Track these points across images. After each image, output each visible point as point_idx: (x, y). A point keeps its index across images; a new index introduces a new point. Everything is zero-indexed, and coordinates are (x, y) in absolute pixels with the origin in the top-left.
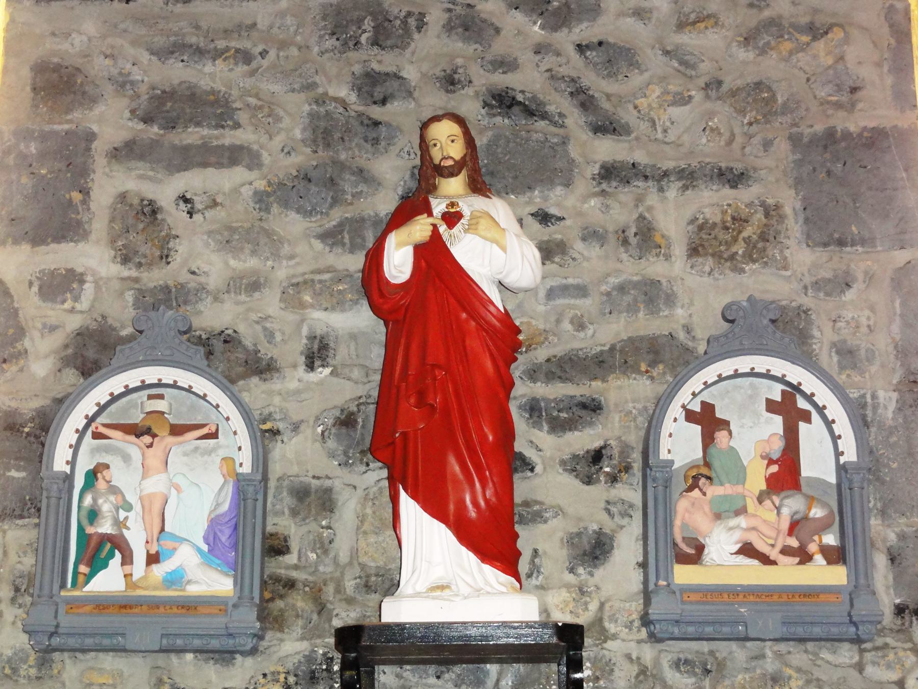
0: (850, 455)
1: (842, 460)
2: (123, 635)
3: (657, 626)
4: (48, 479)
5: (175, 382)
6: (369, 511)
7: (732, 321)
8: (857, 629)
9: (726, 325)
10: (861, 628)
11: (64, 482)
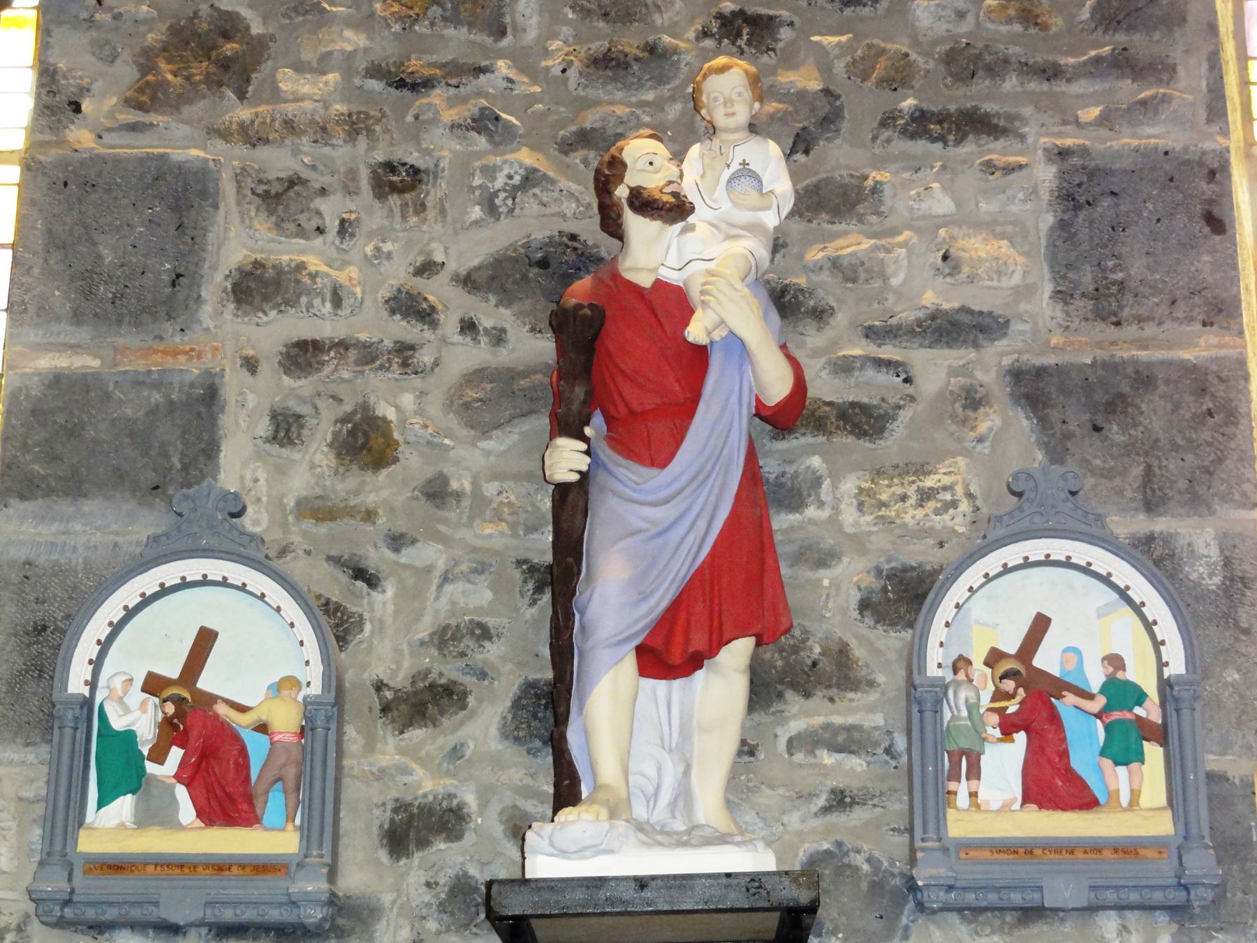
0: (1177, 666)
1: (1167, 672)
2: (156, 904)
3: (925, 894)
4: (61, 703)
5: (225, 578)
6: (871, 802)
7: (1019, 495)
8: (1189, 893)
9: (1015, 499)
10: (1193, 893)
11: (82, 708)
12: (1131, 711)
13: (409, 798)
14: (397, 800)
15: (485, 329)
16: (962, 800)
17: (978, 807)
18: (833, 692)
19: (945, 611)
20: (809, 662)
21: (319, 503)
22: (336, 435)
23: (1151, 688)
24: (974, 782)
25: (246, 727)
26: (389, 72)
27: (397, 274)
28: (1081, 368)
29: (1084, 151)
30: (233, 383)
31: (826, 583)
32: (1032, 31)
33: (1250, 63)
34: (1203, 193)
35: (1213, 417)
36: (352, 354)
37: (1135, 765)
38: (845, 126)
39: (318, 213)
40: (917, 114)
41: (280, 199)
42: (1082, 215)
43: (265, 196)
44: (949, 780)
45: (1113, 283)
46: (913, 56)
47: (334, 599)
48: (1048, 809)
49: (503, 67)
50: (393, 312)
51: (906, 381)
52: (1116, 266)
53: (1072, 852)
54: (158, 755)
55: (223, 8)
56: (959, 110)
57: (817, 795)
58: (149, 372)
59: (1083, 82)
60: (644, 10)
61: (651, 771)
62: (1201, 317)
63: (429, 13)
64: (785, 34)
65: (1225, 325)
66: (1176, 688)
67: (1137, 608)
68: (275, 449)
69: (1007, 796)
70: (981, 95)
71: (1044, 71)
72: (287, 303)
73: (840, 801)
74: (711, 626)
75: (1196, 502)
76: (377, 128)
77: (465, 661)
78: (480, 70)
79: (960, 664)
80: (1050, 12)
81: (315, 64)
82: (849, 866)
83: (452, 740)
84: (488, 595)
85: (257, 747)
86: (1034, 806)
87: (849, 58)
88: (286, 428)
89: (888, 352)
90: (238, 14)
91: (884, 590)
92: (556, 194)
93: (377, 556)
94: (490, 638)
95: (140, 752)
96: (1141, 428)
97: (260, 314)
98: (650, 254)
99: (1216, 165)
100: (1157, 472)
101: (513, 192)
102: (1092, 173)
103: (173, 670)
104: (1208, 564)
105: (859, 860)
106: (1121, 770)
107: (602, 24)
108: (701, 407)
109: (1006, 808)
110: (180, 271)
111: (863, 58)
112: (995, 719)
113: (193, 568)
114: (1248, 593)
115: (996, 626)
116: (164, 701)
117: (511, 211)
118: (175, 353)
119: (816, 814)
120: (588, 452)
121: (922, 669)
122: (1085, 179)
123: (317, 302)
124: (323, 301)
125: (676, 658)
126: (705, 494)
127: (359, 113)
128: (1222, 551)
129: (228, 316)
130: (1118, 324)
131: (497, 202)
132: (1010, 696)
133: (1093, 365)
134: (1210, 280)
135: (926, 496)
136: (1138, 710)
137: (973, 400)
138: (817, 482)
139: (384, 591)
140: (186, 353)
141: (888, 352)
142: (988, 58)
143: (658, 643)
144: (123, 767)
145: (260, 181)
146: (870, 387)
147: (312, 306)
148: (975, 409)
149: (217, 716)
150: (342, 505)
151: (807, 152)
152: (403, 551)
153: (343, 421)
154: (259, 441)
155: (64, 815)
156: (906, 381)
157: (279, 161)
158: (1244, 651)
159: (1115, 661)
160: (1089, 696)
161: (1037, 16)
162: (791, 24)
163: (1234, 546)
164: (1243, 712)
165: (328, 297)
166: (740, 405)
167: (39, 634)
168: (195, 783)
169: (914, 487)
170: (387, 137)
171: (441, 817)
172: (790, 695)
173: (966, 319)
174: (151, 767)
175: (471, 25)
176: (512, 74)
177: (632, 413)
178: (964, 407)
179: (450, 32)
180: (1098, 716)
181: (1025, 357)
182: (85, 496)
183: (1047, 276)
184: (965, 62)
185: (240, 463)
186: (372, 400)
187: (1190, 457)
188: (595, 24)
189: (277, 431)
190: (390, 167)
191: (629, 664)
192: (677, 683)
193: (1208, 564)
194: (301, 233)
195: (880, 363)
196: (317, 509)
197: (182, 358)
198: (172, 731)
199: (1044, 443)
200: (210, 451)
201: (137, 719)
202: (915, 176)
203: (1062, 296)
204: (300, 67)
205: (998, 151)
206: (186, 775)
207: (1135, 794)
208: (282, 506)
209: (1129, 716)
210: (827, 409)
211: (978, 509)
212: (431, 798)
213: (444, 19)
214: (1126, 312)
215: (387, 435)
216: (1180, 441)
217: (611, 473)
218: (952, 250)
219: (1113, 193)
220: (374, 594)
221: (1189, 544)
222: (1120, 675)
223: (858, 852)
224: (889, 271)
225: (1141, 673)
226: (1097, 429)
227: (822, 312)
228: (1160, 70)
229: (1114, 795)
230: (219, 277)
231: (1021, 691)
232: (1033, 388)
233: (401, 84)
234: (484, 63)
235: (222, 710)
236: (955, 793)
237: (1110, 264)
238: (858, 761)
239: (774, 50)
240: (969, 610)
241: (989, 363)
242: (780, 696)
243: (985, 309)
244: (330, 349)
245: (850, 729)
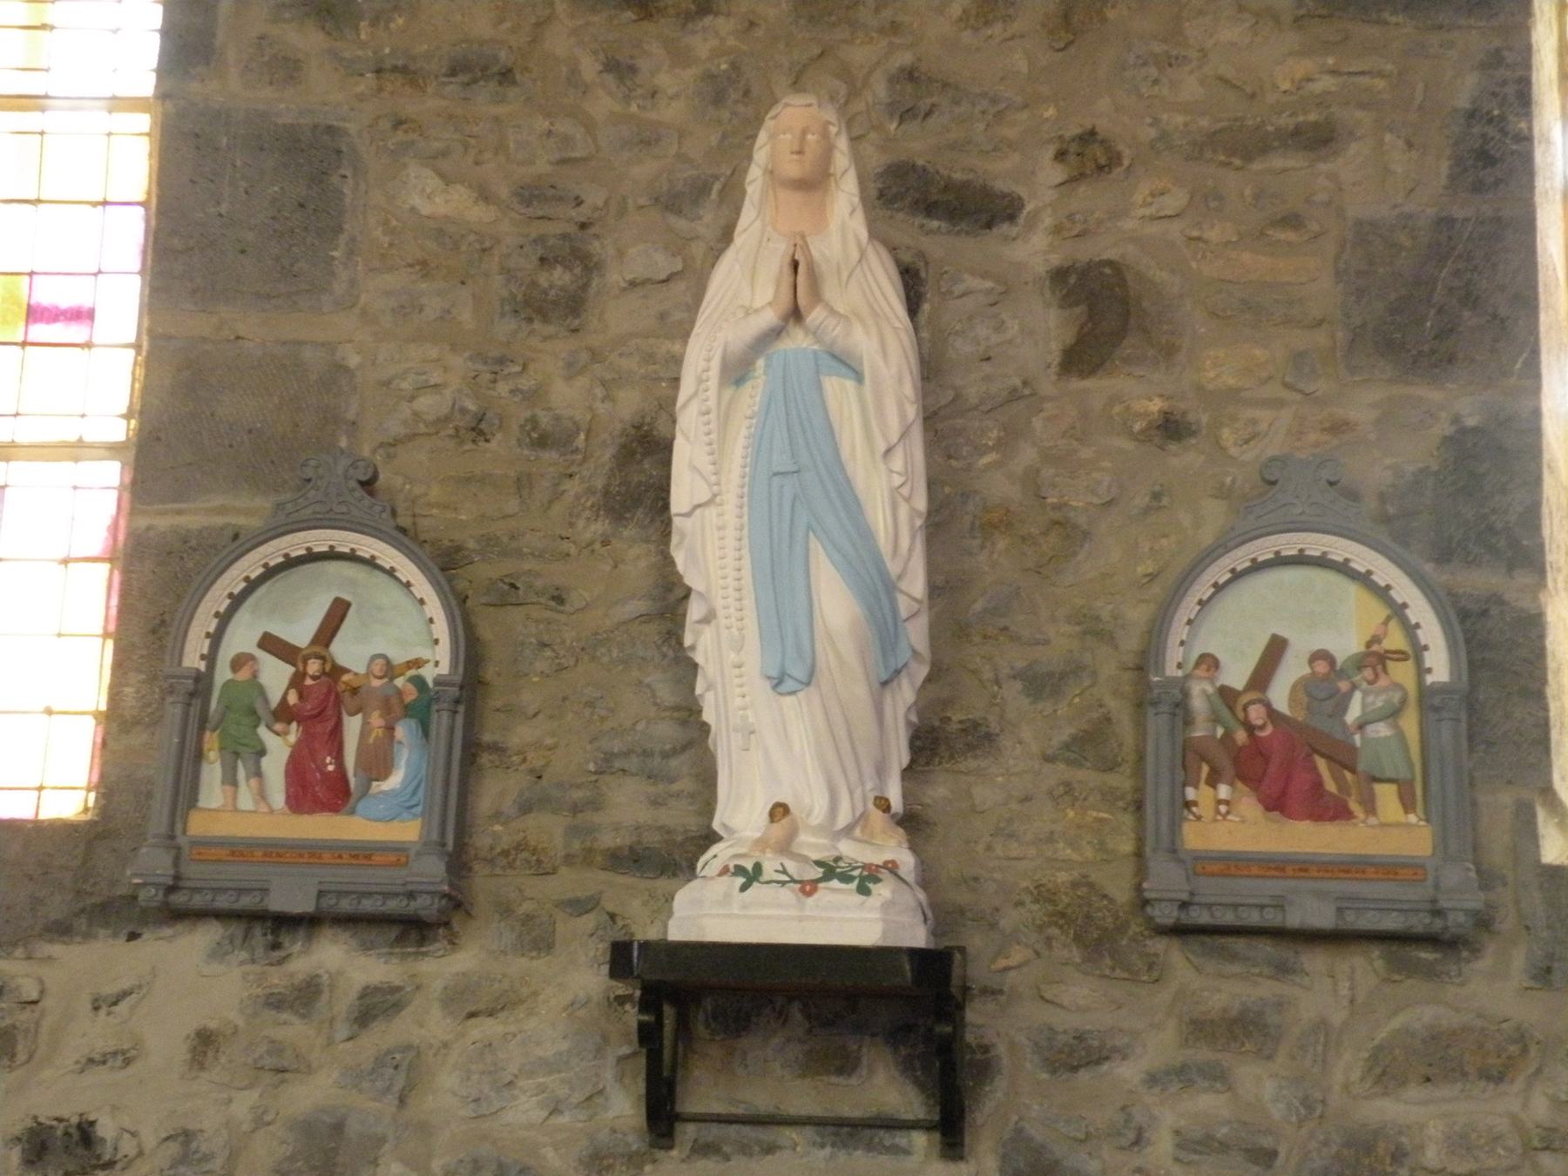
113: (320, 539)
121: (1160, 666)
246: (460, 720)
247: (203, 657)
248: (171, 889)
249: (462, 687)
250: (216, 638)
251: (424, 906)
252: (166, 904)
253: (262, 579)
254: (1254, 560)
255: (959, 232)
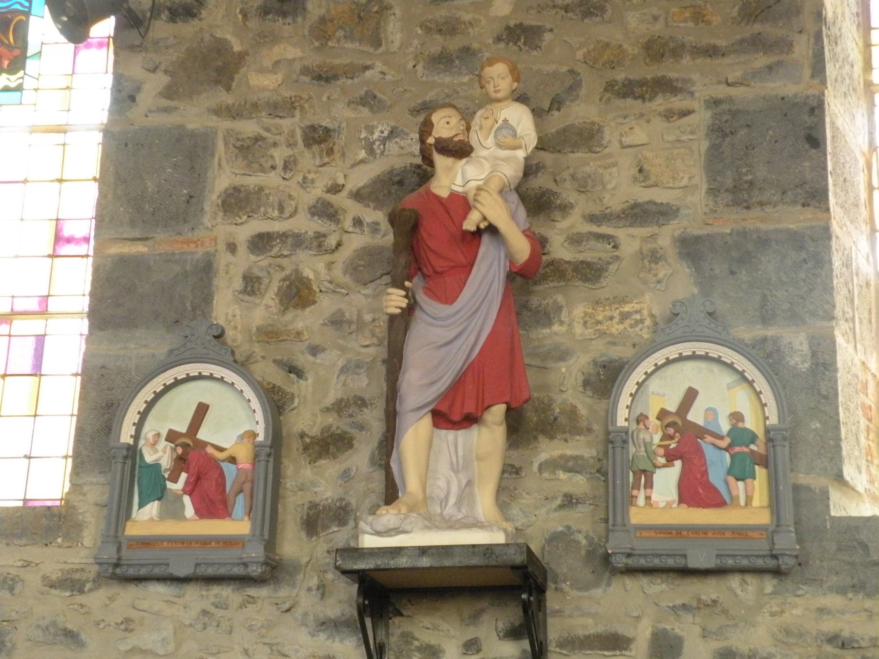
0: (773, 420)
12: (747, 446)
13: (317, 500)
14: (311, 502)
15: (367, 224)
16: (641, 501)
17: (651, 505)
18: (567, 436)
19: (630, 386)
20: (552, 418)
21: (270, 329)
22: (280, 289)
23: (760, 434)
24: (648, 490)
25: (223, 461)
26: (314, 71)
27: (318, 191)
28: (723, 236)
29: (730, 100)
30: (223, 259)
31: (563, 370)
32: (701, 25)
33: (872, 32)
34: (806, 123)
35: (807, 263)
36: (290, 241)
37: (749, 481)
38: (583, 92)
39: (272, 157)
40: (626, 83)
41: (249, 150)
42: (728, 140)
43: (241, 149)
44: (633, 489)
45: (746, 182)
46: (625, 46)
47: (278, 384)
48: (693, 506)
49: (379, 66)
50: (313, 214)
51: (614, 247)
52: (747, 171)
53: (706, 534)
54: (174, 479)
55: (217, 36)
56: (653, 79)
57: (556, 498)
58: (174, 254)
59: (732, 56)
60: (463, 26)
61: (442, 483)
62: (802, 201)
63: (337, 34)
64: (547, 37)
65: (818, 205)
66: (772, 433)
67: (751, 383)
68: (247, 298)
69: (670, 499)
70: (670, 70)
71: (707, 51)
72: (252, 212)
73: (570, 501)
74: (478, 397)
75: (795, 318)
76: (306, 105)
77: (352, 419)
78: (367, 68)
79: (641, 419)
80: (712, 13)
81: (271, 68)
82: (574, 541)
83: (344, 466)
84: (365, 381)
85: (229, 470)
86: (685, 506)
87: (585, 50)
88: (251, 285)
89: (604, 229)
90: (226, 39)
91: (598, 374)
92: (409, 141)
93: (303, 359)
94: (366, 407)
95: (164, 476)
96: (760, 272)
97: (237, 218)
98: (452, 178)
99: (815, 104)
100: (770, 298)
101: (384, 141)
102: (734, 114)
103: (183, 428)
104: (802, 356)
105: (580, 538)
106: (741, 484)
107: (438, 37)
108: (475, 268)
109: (669, 504)
110: (192, 194)
111: (594, 50)
112: (661, 451)
113: (193, 369)
114: (827, 373)
115: (664, 395)
116: (177, 446)
117: (382, 153)
118: (188, 242)
119: (555, 510)
120: (406, 297)
121: (614, 421)
122: (729, 117)
123: (270, 210)
124: (273, 210)
125: (456, 418)
126: (475, 321)
127: (295, 97)
128: (810, 347)
129: (219, 220)
130: (748, 208)
131: (374, 147)
132: (672, 438)
133: (730, 234)
134: (808, 177)
135: (624, 316)
136: (753, 447)
137: (655, 257)
138: (560, 309)
139: (306, 380)
140: (194, 242)
141: (604, 229)
142: (672, 45)
143: (444, 409)
144: (154, 486)
145: (238, 140)
146: (593, 253)
147: (267, 213)
148: (657, 263)
149: (206, 454)
150: (284, 329)
151: (559, 109)
152: (318, 356)
153: (284, 280)
154: (236, 293)
155: (121, 512)
156: (614, 247)
157: (249, 128)
158: (823, 409)
159: (737, 417)
160: (721, 438)
161: (704, 16)
162: (551, 30)
163: (819, 344)
164: (822, 447)
165: (276, 207)
166: (499, 268)
167: (109, 408)
168: (195, 493)
169: (618, 311)
170: (312, 111)
171: (336, 512)
172: (541, 438)
173: (653, 208)
174: (170, 485)
175: (360, 41)
176: (384, 68)
177: (436, 272)
178: (650, 262)
179: (349, 45)
180: (726, 449)
181: (689, 230)
182: (137, 327)
183: (705, 179)
184: (656, 49)
185: (226, 308)
186: (301, 267)
187: (791, 289)
188: (434, 37)
189: (246, 287)
190: (313, 128)
191: (427, 421)
192: (461, 433)
193: (802, 356)
194: (263, 170)
195: (600, 237)
196: (269, 334)
197: (192, 245)
198: (181, 462)
199: (699, 283)
200: (207, 299)
201: (162, 457)
202: (624, 121)
203: (713, 192)
204: (262, 71)
205: (678, 102)
206: (191, 489)
207: (749, 499)
208: (250, 331)
209: (746, 450)
210: (567, 266)
211: (657, 324)
212: (330, 501)
213: (345, 37)
214: (754, 200)
215: (310, 288)
216: (784, 279)
217: (424, 311)
218: (645, 166)
219: (748, 126)
220: (301, 381)
221: (790, 343)
222: (740, 425)
223: (580, 532)
224: (606, 180)
225: (751, 423)
226: (732, 273)
227: (565, 206)
228: (787, 46)
229: (734, 499)
230: (214, 197)
231: (677, 434)
232: (691, 248)
233: (319, 78)
234: (369, 63)
235: (210, 450)
236: (636, 497)
237: (744, 170)
238: (582, 477)
239: (540, 47)
240: (648, 385)
241: (665, 237)
242: (536, 438)
243: (664, 202)
244: (277, 238)
245: (576, 458)
246: (271, 465)
247: (131, 436)
248: (117, 565)
249: (271, 447)
250: (139, 426)
251: (255, 570)
252: (114, 573)
253: (675, 361)
254: (667, 358)
255: (317, 202)
